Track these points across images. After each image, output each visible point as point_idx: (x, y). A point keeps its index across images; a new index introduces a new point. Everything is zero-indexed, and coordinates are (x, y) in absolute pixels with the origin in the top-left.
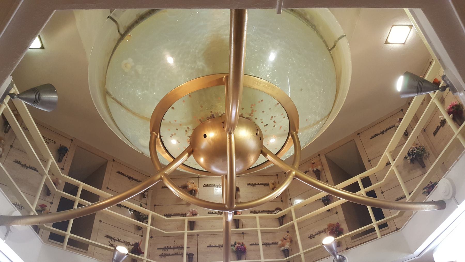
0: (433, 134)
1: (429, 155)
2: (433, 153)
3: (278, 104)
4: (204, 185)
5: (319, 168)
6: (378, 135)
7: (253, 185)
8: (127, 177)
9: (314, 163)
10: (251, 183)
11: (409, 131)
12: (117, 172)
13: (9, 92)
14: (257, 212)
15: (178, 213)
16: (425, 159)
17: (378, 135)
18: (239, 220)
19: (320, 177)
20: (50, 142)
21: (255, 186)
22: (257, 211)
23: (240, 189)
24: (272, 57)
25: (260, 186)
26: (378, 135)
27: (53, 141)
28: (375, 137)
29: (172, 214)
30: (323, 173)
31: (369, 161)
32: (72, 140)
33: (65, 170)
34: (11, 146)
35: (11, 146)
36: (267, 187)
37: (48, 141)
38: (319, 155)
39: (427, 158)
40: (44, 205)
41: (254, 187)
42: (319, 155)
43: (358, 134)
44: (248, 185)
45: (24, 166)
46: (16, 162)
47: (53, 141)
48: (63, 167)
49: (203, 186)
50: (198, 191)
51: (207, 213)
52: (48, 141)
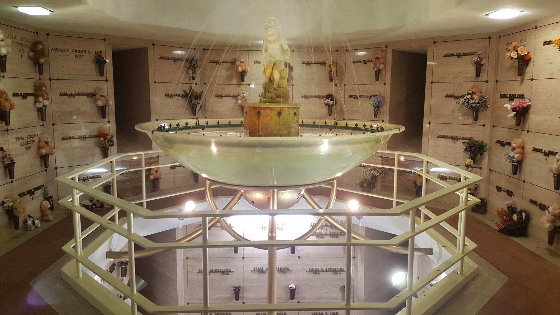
0: (500, 95)
1: (488, 109)
2: (492, 108)
3: (261, 271)
4: (255, 62)
5: (381, 67)
6: (451, 56)
7: (309, 64)
8: (171, 59)
9: (378, 58)
10: (306, 61)
11: (484, 70)
12: (160, 59)
13: (62, 269)
14: (308, 97)
15: (229, 94)
16: (482, 111)
17: (452, 55)
18: (241, 289)
19: (380, 75)
20: (84, 54)
21: (310, 65)
22: (309, 96)
23: (294, 69)
24: (276, 183)
25: (317, 64)
26: (452, 55)
27: (87, 52)
28: (449, 56)
29: (223, 95)
30: (384, 73)
31: (432, 83)
32: (105, 40)
33: (109, 80)
34: (50, 79)
35: (50, 79)
36: (323, 67)
37: (82, 54)
38: (387, 47)
39: (484, 111)
40: (110, 267)
41: (310, 66)
42: (387, 47)
43: (434, 42)
44: (303, 63)
45: (71, 95)
46: (62, 94)
47: (87, 52)
48: (106, 78)
49: (254, 63)
50: (249, 72)
51: (259, 96)
52: (82, 54)
